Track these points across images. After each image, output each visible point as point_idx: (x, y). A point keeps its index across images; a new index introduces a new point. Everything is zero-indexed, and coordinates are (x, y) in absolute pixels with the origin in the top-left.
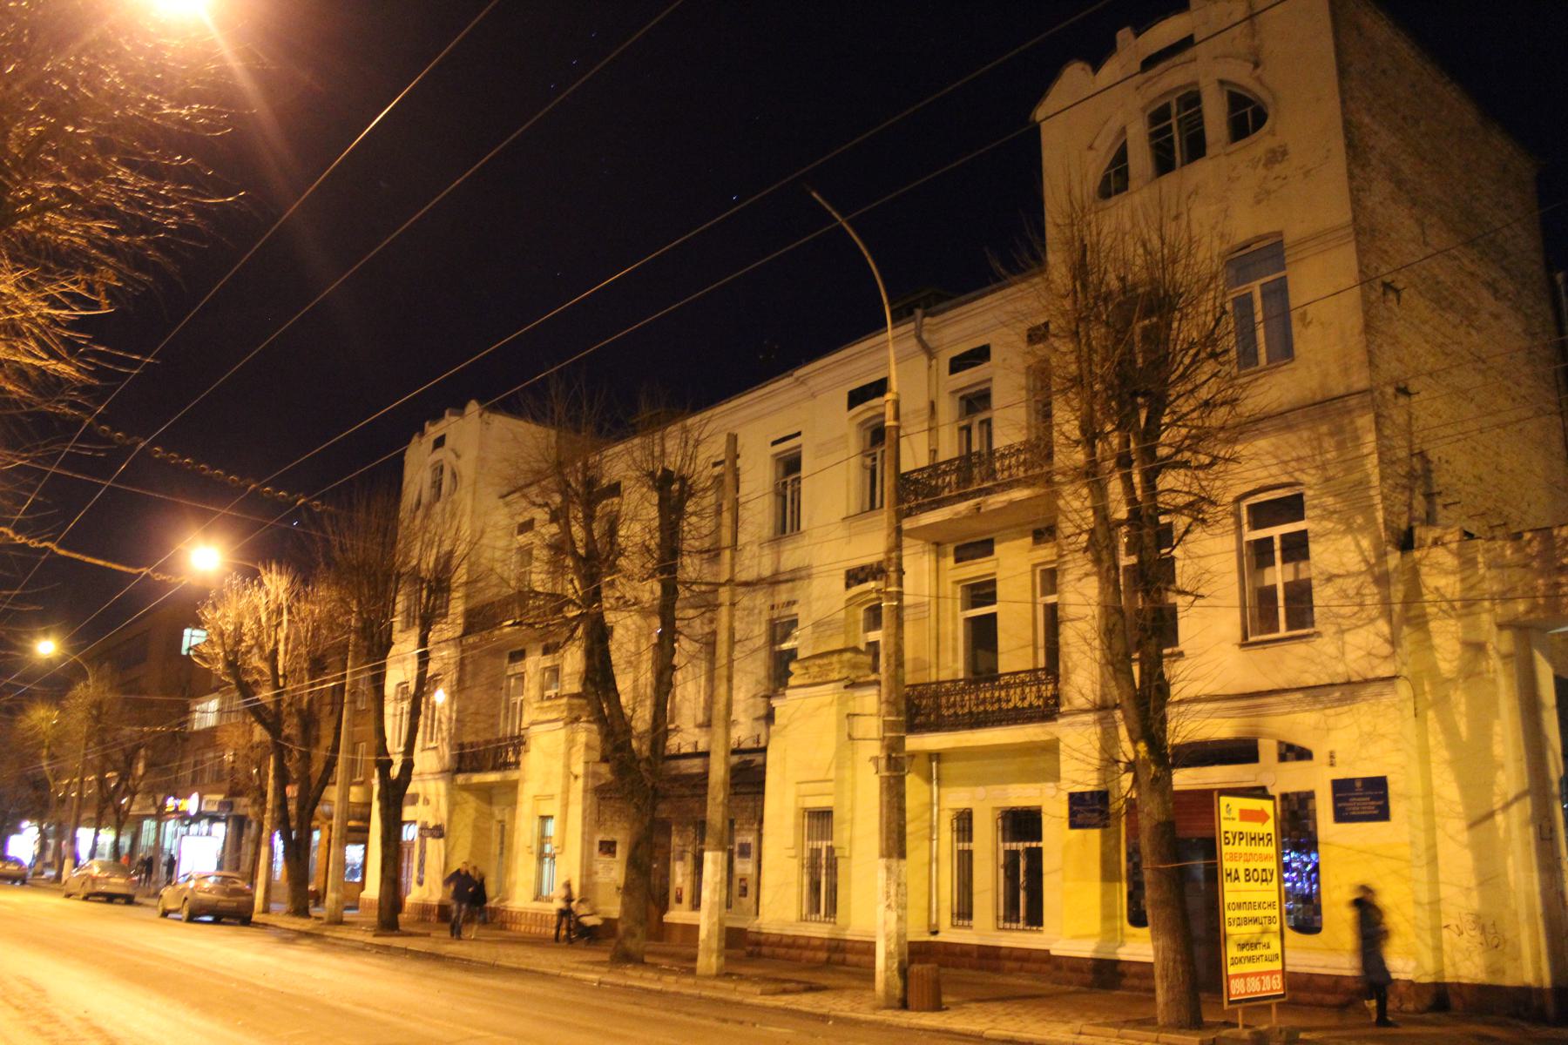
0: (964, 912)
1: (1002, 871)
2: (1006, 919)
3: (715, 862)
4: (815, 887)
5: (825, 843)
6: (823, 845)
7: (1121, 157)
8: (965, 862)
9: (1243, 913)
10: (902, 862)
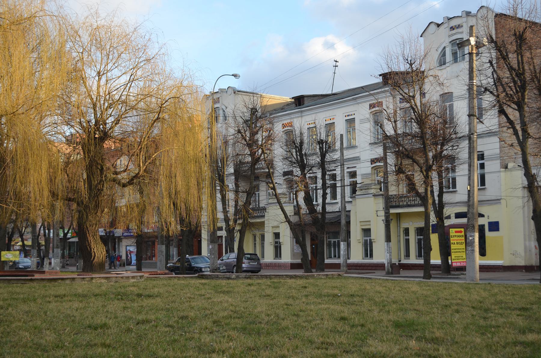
0: (408, 255)
1: (417, 244)
3: (344, 245)
4: (366, 250)
6: (368, 238)
7: (444, 54)
8: (407, 242)
9: (454, 251)
10: (390, 243)
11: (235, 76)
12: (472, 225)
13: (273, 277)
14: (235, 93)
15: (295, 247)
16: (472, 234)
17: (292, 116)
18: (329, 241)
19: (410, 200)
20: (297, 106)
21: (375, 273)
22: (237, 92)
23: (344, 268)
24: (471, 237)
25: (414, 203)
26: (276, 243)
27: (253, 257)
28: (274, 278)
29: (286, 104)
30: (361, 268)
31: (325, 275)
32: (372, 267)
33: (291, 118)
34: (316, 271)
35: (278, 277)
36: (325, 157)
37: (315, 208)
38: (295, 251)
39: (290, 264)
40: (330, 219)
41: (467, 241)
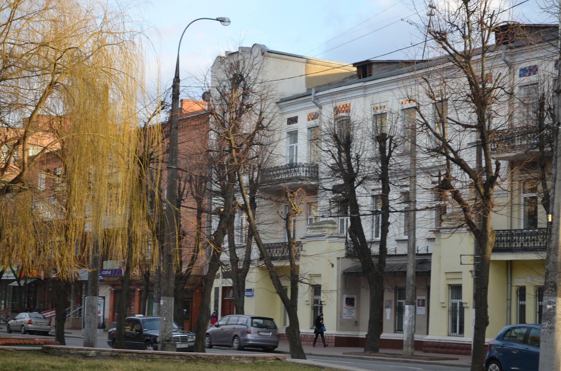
2: (452, 332)
3: (410, 310)
4: (454, 321)
5: (458, 300)
11: (221, 20)
12: (552, 284)
13: (158, 357)
14: (263, 54)
15: (345, 311)
16: (552, 300)
17: (349, 95)
18: (399, 303)
19: (503, 240)
20: (360, 78)
21: (458, 359)
22: (266, 53)
23: (408, 349)
24: (550, 304)
25: (533, 245)
26: (316, 301)
27: (269, 323)
28: (160, 358)
29: (349, 76)
30: (443, 350)
31: (250, 358)
32: (462, 349)
33: (346, 99)
34: (365, 351)
35: (166, 357)
36: (387, 163)
37: (369, 247)
38: (344, 317)
39: (334, 338)
40: (392, 266)
41: (544, 311)
